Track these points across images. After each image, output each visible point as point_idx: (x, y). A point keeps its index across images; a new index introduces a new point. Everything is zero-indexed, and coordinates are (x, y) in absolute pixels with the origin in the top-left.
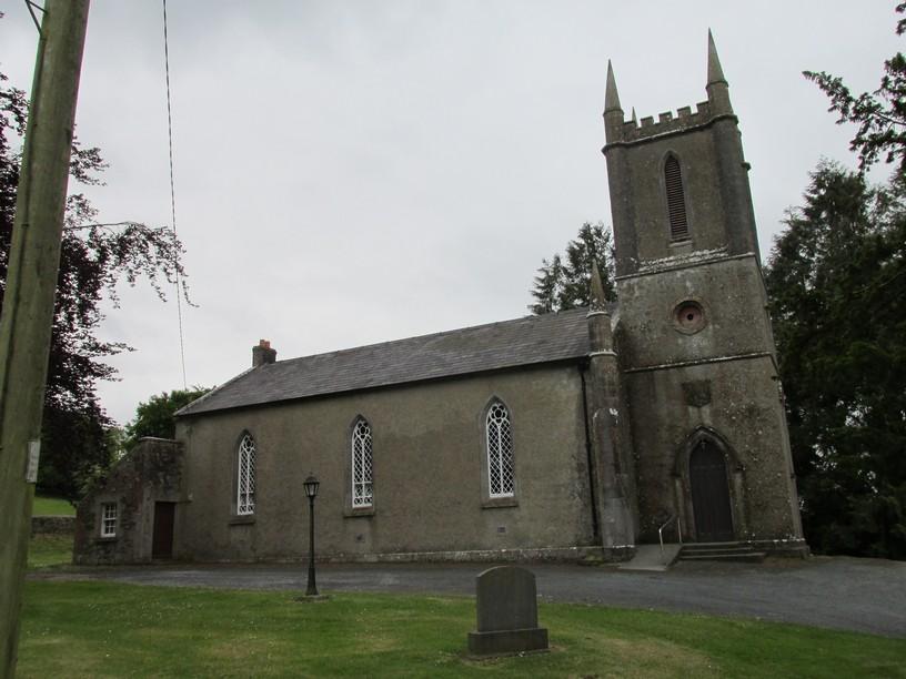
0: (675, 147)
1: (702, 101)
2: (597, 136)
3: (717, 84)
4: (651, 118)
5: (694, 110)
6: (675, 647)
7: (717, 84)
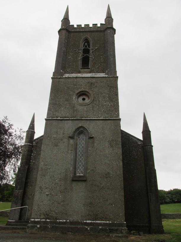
0: (88, 36)
3: (109, 18)
5: (99, 25)
7: (109, 18)
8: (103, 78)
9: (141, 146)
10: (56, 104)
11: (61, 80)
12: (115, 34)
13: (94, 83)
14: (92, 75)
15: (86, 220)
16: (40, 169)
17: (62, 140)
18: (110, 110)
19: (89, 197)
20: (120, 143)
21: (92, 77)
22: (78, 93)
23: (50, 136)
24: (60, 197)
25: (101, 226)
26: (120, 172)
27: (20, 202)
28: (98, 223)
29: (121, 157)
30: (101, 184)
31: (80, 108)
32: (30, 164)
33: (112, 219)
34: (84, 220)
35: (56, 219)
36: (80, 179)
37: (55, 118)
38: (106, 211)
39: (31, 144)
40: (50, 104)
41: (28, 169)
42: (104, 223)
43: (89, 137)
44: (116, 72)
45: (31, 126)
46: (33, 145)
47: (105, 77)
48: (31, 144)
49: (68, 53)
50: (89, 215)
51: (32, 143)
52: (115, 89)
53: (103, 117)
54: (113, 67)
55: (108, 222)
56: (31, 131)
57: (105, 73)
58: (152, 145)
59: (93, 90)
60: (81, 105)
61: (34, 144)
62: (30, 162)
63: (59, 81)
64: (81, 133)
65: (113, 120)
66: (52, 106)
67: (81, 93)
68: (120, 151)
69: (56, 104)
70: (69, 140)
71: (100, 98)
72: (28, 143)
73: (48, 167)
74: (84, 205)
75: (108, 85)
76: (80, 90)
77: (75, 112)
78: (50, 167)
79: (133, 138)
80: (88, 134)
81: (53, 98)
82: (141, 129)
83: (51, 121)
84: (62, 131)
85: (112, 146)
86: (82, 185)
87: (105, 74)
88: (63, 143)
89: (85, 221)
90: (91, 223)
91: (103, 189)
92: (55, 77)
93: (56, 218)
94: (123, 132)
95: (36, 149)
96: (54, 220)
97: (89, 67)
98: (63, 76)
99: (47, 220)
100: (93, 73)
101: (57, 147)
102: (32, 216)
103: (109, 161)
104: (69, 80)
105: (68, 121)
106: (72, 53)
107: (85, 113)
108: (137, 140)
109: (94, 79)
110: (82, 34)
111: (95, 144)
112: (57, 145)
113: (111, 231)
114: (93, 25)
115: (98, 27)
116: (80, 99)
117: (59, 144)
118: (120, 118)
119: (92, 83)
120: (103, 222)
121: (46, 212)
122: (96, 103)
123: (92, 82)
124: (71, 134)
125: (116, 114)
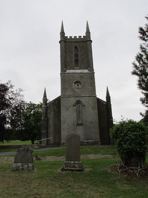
0: (77, 44)
1: (84, 36)
2: (58, 38)
3: (88, 32)
4: (72, 37)
5: (82, 37)
6: (79, 172)
7: (88, 32)
11: (65, 74)
12: (92, 43)
15: (84, 141)
16: (62, 121)
17: (70, 107)
18: (91, 91)
26: (97, 120)
27: (46, 137)
29: (97, 114)
31: (77, 90)
36: (81, 124)
40: (62, 88)
41: (47, 119)
44: (94, 69)
50: (85, 139)
51: (47, 106)
54: (92, 66)
60: (77, 89)
62: (47, 116)
64: (79, 103)
67: (76, 82)
68: (97, 111)
69: (65, 88)
70: (73, 107)
72: (45, 105)
74: (83, 135)
75: (90, 77)
76: (76, 80)
77: (75, 92)
78: (66, 120)
79: (101, 101)
81: (63, 85)
82: (105, 96)
83: (64, 98)
84: (69, 103)
85: (93, 109)
86: (81, 127)
88: (71, 108)
90: (86, 142)
94: (97, 98)
102: (62, 141)
103: (91, 115)
107: (79, 93)
108: (103, 102)
109: (83, 74)
110: (73, 43)
111: (86, 109)
113: (95, 144)
114: (79, 36)
116: (76, 84)
117: (69, 109)
119: (81, 77)
123: (82, 75)
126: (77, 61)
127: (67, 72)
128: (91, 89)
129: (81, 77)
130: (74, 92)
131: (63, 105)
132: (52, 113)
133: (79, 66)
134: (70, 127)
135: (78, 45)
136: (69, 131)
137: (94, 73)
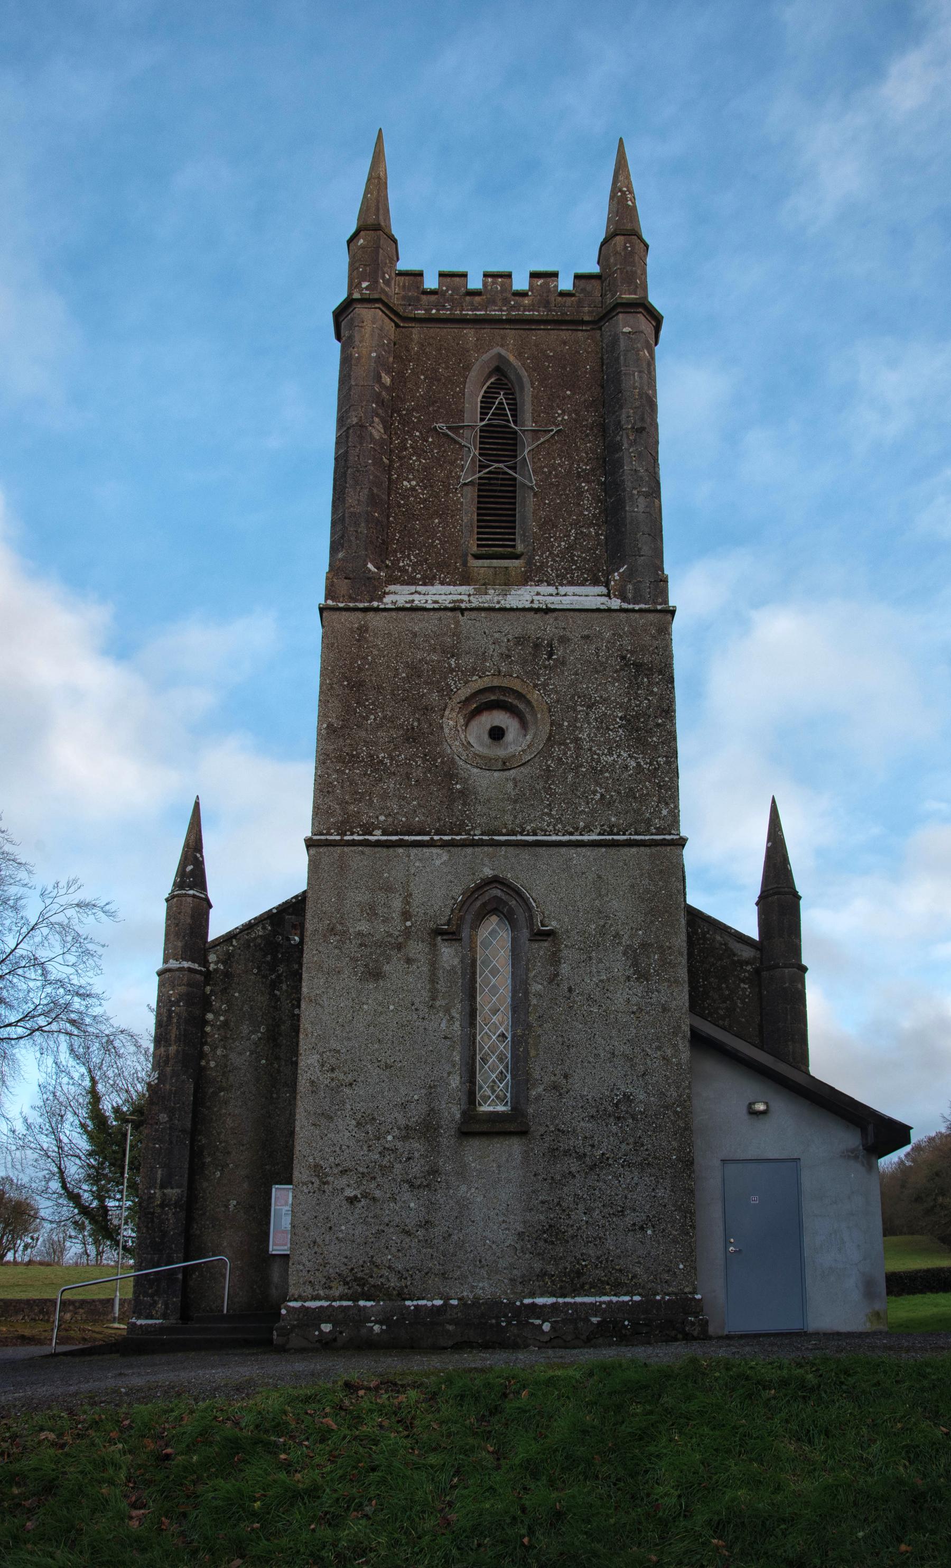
3: (624, 237)
5: (565, 283)
7: (624, 237)
8: (596, 615)
9: (749, 968)
10: (353, 759)
11: (375, 621)
13: (550, 645)
14: (538, 594)
15: (532, 1295)
17: (399, 947)
19: (543, 1202)
20: (680, 959)
21: (537, 610)
22: (468, 700)
23: (339, 927)
24: (412, 1205)
25: (596, 1316)
28: (584, 1304)
30: (593, 1146)
32: (203, 1063)
33: (643, 1288)
34: (525, 1297)
35: (402, 1296)
37: (356, 837)
38: (619, 1257)
39: (196, 966)
42: (611, 1302)
43: (532, 930)
44: (665, 580)
45: (190, 868)
46: (208, 969)
47: (609, 610)
48: (196, 966)
49: (400, 458)
50: (543, 1274)
51: (205, 963)
52: (657, 678)
53: (598, 831)
54: (646, 550)
55: (627, 1298)
56: (194, 896)
57: (607, 585)
58: (805, 961)
59: (545, 685)
60: (488, 764)
61: (212, 967)
62: (202, 1055)
63: (363, 629)
65: (649, 846)
66: (337, 771)
70: (434, 946)
71: (581, 730)
72: (184, 959)
73: (342, 1076)
76: (478, 683)
80: (531, 917)
83: (339, 850)
84: (397, 904)
85: (643, 976)
86: (510, 1151)
87: (602, 589)
89: (527, 1301)
90: (553, 1305)
91: (602, 1168)
92: (341, 605)
93: (399, 1294)
95: (224, 991)
96: (390, 1300)
97: (520, 548)
98: (380, 599)
99: (362, 1303)
100: (539, 583)
101: (377, 980)
102: (292, 1291)
104: (418, 624)
105: (425, 850)
106: (419, 456)
109: (550, 618)
110: (470, 334)
111: (565, 969)
112: (376, 974)
114: (534, 275)
115: (563, 294)
117: (386, 968)
118: (683, 833)
120: (606, 1299)
121: (352, 1269)
122: (565, 754)
124: (444, 920)
125: (665, 812)
126: (498, 508)
127: (388, 599)
128: (626, 767)
129: (537, 646)
130: (452, 801)
131: (332, 930)
132: (245, 1029)
133: (520, 548)
134: (394, 1151)
135: (520, 356)
136: (378, 1194)
137: (672, 612)
